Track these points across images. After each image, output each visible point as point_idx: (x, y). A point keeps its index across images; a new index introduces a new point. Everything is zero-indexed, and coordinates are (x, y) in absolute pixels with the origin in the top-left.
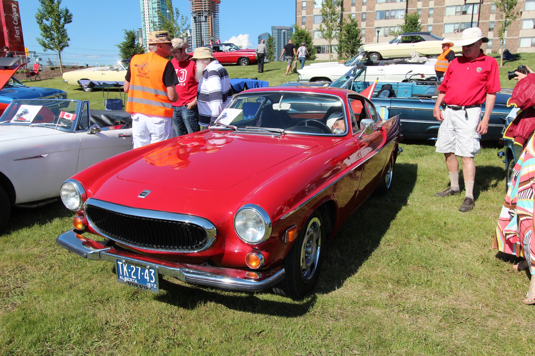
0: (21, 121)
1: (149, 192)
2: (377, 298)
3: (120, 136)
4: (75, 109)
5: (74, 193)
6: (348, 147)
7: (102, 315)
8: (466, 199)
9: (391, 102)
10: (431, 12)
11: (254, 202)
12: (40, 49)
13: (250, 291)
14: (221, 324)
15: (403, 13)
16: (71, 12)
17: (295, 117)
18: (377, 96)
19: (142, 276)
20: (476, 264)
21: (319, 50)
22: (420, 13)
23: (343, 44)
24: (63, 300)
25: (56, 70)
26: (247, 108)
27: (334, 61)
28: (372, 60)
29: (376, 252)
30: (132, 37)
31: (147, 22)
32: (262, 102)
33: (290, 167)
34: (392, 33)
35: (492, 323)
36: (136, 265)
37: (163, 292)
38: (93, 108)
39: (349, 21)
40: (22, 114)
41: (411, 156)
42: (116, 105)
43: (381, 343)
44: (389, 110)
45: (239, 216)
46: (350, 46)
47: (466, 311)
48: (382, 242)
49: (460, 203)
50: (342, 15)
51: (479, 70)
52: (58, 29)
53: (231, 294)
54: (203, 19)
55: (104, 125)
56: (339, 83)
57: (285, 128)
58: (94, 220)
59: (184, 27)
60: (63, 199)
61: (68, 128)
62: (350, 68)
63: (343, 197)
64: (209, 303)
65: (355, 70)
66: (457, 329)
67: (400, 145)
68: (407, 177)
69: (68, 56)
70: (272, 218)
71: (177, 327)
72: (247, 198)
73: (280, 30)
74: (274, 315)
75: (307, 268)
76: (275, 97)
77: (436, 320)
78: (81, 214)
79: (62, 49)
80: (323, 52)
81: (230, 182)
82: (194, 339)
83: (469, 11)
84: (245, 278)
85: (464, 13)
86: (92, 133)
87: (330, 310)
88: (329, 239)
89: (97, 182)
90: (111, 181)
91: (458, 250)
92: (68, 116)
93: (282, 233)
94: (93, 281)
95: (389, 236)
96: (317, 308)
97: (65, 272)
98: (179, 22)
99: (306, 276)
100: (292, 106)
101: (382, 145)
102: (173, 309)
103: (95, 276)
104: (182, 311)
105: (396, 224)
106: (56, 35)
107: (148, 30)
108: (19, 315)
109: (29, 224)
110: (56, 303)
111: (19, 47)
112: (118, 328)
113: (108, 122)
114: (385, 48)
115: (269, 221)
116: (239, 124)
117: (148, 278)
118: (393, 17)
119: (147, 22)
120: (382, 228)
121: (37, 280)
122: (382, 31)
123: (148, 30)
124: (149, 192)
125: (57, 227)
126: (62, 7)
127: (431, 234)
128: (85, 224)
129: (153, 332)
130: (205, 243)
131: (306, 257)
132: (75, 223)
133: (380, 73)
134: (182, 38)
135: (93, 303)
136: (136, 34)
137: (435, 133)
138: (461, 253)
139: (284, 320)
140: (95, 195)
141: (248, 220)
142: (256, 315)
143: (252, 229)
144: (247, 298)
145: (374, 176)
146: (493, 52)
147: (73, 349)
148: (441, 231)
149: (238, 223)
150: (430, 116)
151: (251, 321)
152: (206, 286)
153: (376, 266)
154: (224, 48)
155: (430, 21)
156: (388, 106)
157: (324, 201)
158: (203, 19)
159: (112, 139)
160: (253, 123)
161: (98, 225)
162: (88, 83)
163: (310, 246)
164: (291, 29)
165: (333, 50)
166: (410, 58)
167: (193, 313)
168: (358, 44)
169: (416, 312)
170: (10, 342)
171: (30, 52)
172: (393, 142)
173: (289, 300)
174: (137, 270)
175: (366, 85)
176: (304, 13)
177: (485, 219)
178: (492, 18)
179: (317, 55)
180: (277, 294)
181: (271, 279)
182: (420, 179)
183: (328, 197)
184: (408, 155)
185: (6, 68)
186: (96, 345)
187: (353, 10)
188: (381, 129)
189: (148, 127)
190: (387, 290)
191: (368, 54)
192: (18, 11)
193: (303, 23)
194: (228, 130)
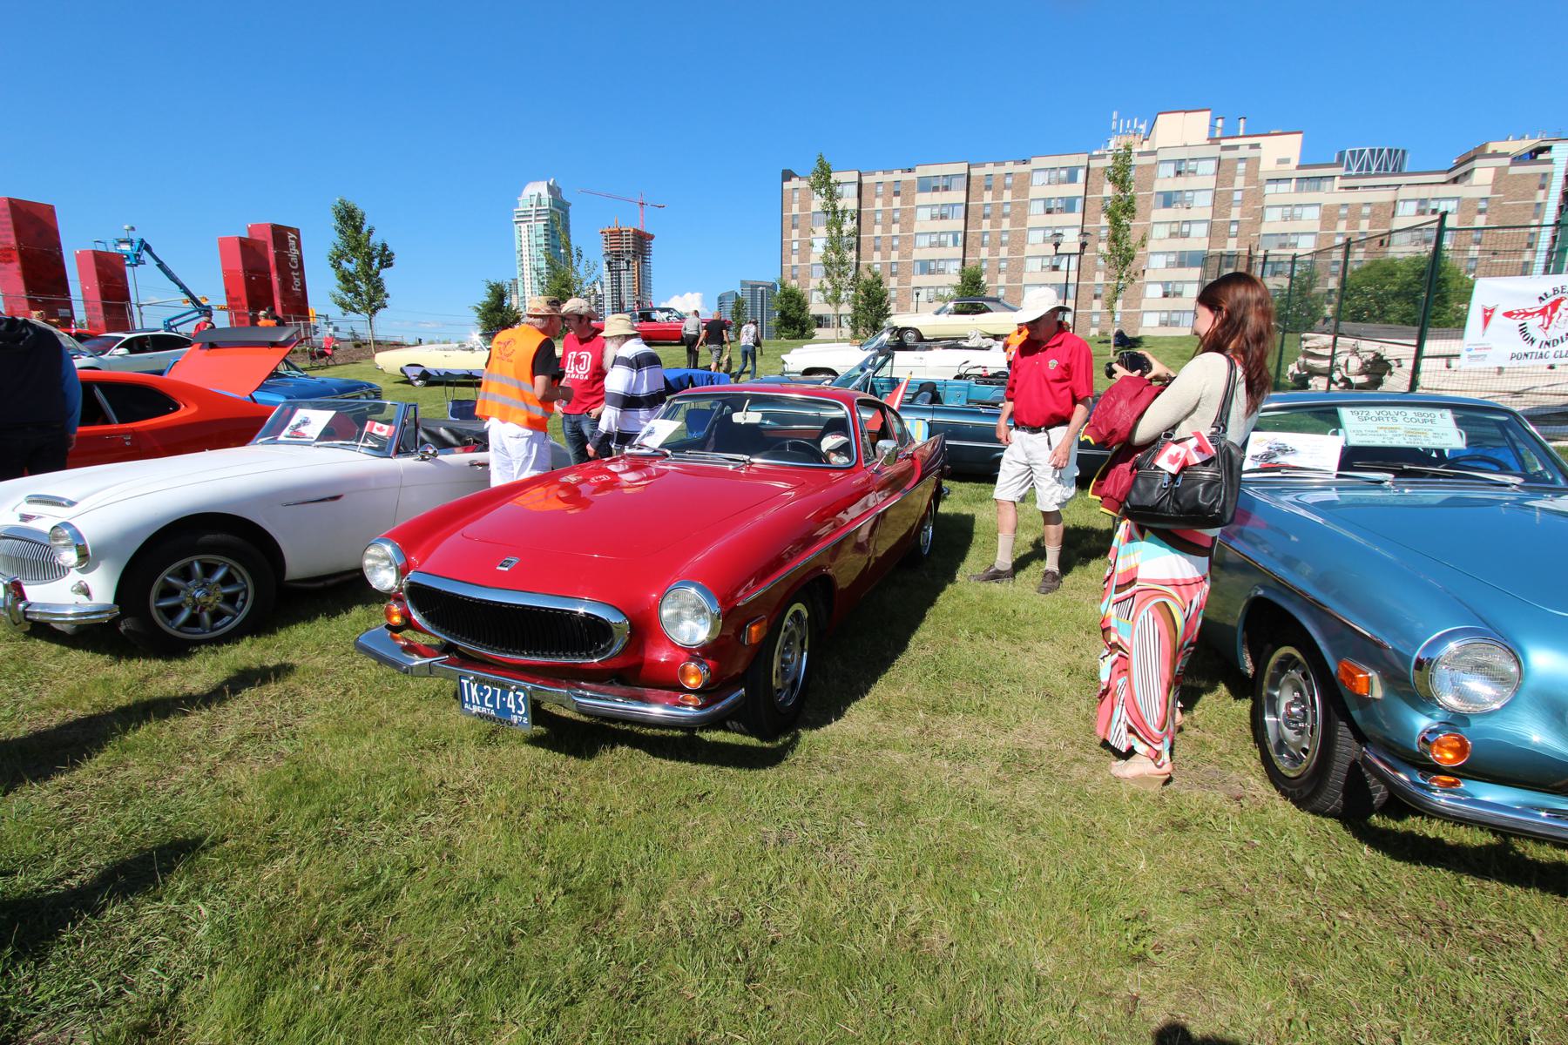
0: (298, 438)
1: (515, 560)
2: (899, 735)
3: (472, 464)
4: (393, 417)
5: (386, 563)
6: (857, 486)
7: (434, 770)
8: (1047, 573)
9: (933, 411)
10: (1003, 265)
11: (692, 579)
12: (336, 312)
13: (688, 727)
14: (637, 783)
15: (958, 265)
16: (391, 248)
17: (773, 435)
18: (911, 402)
19: (503, 704)
20: (1060, 677)
21: (821, 321)
22: (984, 266)
23: (861, 314)
24: (366, 746)
25: (363, 347)
26: (693, 419)
27: (844, 340)
28: (904, 341)
29: (902, 659)
30: (499, 294)
31: (527, 268)
32: (717, 408)
33: (760, 518)
34: (940, 298)
35: (1079, 771)
36: (493, 684)
37: (540, 730)
38: (428, 416)
39: (868, 276)
40: (298, 426)
41: (965, 501)
42: (465, 410)
43: (902, 808)
44: (930, 424)
45: (669, 599)
46: (871, 317)
47: (1040, 753)
48: (911, 644)
49: (1039, 579)
50: (858, 265)
51: (1053, 364)
52: (368, 277)
53: (657, 732)
54: (623, 265)
55: (444, 445)
56: (849, 379)
57: (751, 454)
58: (420, 609)
59: (590, 280)
60: (367, 572)
61: (381, 449)
62: (869, 353)
63: (846, 571)
64: (619, 748)
65: (875, 358)
66: (1024, 783)
67: (946, 484)
68: (956, 537)
69: (385, 324)
70: (724, 601)
71: (563, 789)
72: (685, 569)
73: (754, 287)
74: (727, 765)
75: (785, 686)
76: (737, 403)
77: (991, 767)
78: (398, 599)
79: (374, 311)
80: (827, 326)
81: (648, 547)
82: (591, 808)
83: (1063, 266)
84: (679, 704)
85: (1056, 268)
86: (423, 459)
87: (822, 756)
88: (823, 641)
89: (427, 543)
90: (451, 543)
91: (1032, 655)
92: (380, 429)
93: (741, 629)
94: (419, 714)
95: (924, 632)
96: (800, 754)
97: (371, 699)
98: (582, 270)
99: (785, 701)
100: (765, 417)
101: (912, 483)
102: (557, 758)
103: (424, 704)
104: (573, 762)
105: (935, 614)
106: (364, 287)
107: (527, 282)
108: (289, 772)
109: (309, 617)
110: (353, 751)
111: (298, 306)
112: (461, 792)
113: (452, 439)
114: (927, 321)
115: (716, 610)
116: (676, 446)
117: (513, 707)
118: (942, 271)
119: (527, 268)
120: (913, 620)
121: (321, 713)
122: (923, 293)
123: (527, 282)
124: (515, 560)
125: (358, 621)
126: (376, 240)
127: (991, 630)
128: (406, 615)
129: (522, 798)
130: (611, 646)
131: (783, 669)
132: (389, 614)
133: (917, 362)
134: (587, 297)
135: (419, 751)
136: (507, 288)
137: (997, 463)
138: (1037, 660)
139: (745, 774)
140: (428, 561)
141: (683, 606)
142: (698, 767)
143: (689, 621)
144: (683, 738)
145: (902, 533)
146: (1101, 333)
147: (382, 829)
148: (1008, 626)
149: (666, 612)
150: (990, 435)
151: (688, 776)
152: (614, 719)
153: (900, 684)
154: (657, 316)
155: (1002, 279)
156: (929, 418)
157: (813, 576)
158: (623, 265)
159: (458, 468)
160: (700, 445)
161: (427, 617)
162: (418, 371)
163: (789, 651)
164: (774, 287)
165: (844, 323)
166: (967, 339)
167: (593, 764)
168: (884, 314)
169: (961, 756)
170: (273, 818)
171: (319, 316)
172: (931, 480)
173: (753, 741)
174: (495, 693)
175: (894, 383)
176: (795, 260)
177: (1078, 605)
178: (1100, 278)
179: (817, 331)
180: (734, 731)
181: (719, 707)
182: (978, 539)
183: (819, 568)
184: (958, 499)
185: (274, 345)
186: (421, 820)
187: (877, 256)
188: (912, 457)
189: (510, 452)
190: (915, 721)
191: (901, 332)
192: (298, 246)
193: (793, 277)
194: (658, 455)
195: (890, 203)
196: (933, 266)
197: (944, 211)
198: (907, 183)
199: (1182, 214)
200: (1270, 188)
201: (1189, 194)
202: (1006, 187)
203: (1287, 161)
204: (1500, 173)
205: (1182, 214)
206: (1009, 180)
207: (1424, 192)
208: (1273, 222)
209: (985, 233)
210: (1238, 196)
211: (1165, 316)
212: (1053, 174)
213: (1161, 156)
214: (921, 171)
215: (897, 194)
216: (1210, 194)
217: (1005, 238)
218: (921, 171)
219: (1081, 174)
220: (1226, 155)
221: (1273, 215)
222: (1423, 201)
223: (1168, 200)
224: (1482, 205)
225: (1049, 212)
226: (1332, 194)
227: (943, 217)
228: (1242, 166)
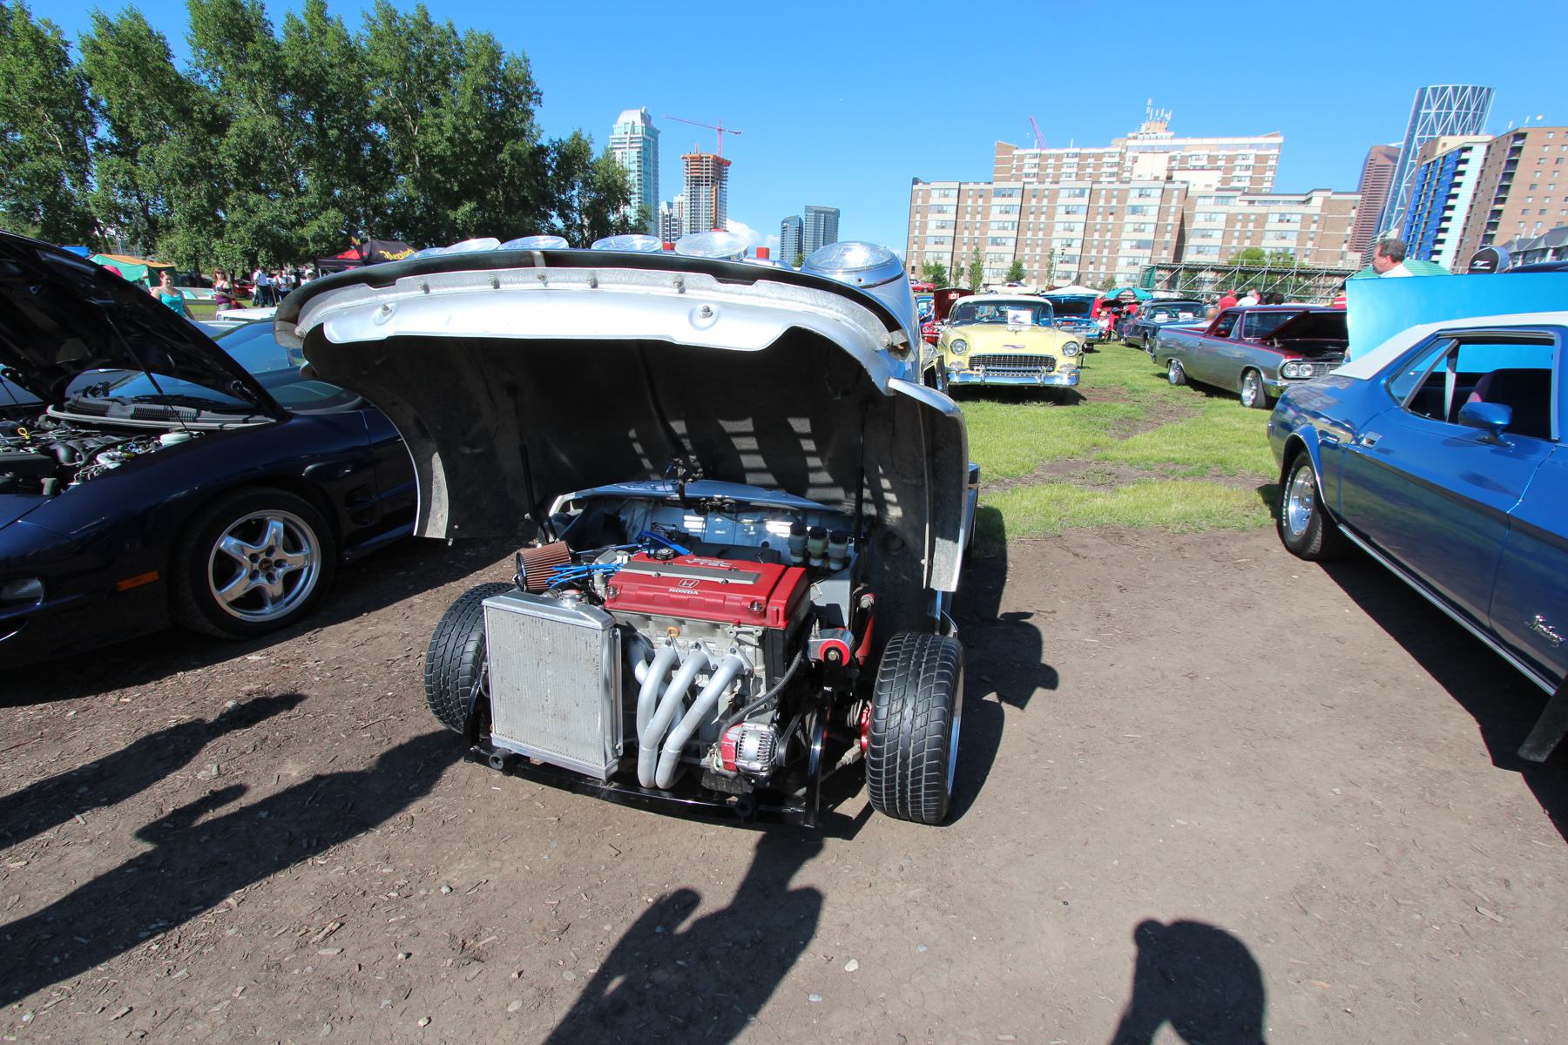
73: (818, 212)
176: (916, 232)
187: (966, 233)
204: (1326, 200)
207: (1282, 208)
214: (996, 185)
218: (996, 185)
223: (1135, 210)
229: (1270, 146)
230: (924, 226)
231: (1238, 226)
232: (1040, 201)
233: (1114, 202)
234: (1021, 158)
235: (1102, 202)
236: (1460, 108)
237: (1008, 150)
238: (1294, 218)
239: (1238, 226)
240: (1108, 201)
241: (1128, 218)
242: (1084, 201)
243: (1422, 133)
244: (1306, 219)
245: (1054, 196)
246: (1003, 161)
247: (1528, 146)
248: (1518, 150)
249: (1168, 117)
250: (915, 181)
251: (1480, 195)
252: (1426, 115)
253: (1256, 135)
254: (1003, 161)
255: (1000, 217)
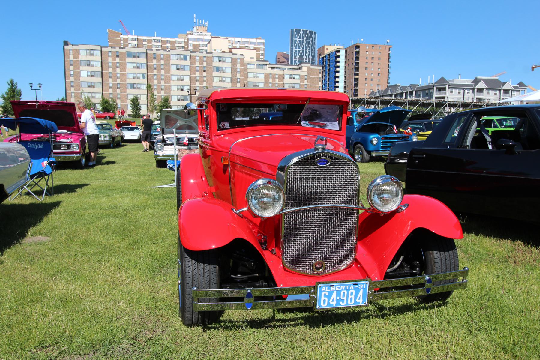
10: (163, 87)
187: (111, 80)
195: (115, 60)
196: (135, 86)
197: (138, 65)
198: (122, 53)
199: (222, 75)
200: (249, 66)
201: (224, 68)
202: (162, 59)
203: (252, 58)
205: (222, 75)
206: (162, 56)
207: (291, 72)
208: (251, 78)
209: (155, 75)
210: (238, 70)
211: (179, 77)
212: (88, 52)
213: (214, 54)
215: (118, 56)
216: (230, 69)
217: (163, 77)
219: (188, 57)
220: (234, 56)
221: (251, 75)
222: (291, 75)
223: (218, 69)
224: (306, 77)
225: (178, 69)
226: (268, 70)
227: (138, 68)
228: (239, 60)
229: (259, 44)
230: (77, 75)
231: (271, 81)
232: (159, 61)
233: (205, 64)
234: (126, 40)
235: (198, 64)
236: (307, 39)
237: (118, 35)
238: (296, 77)
239: (271, 81)
240: (201, 63)
241: (215, 74)
242: (187, 62)
243: (296, 48)
244: (302, 77)
245: (167, 59)
246: (114, 41)
247: (361, 50)
248: (358, 53)
249: (207, 24)
250: (66, 43)
251: (347, 72)
252: (296, 41)
253: (253, 38)
254: (114, 41)
255: (133, 71)
